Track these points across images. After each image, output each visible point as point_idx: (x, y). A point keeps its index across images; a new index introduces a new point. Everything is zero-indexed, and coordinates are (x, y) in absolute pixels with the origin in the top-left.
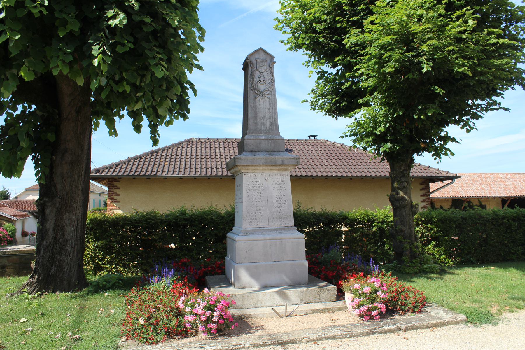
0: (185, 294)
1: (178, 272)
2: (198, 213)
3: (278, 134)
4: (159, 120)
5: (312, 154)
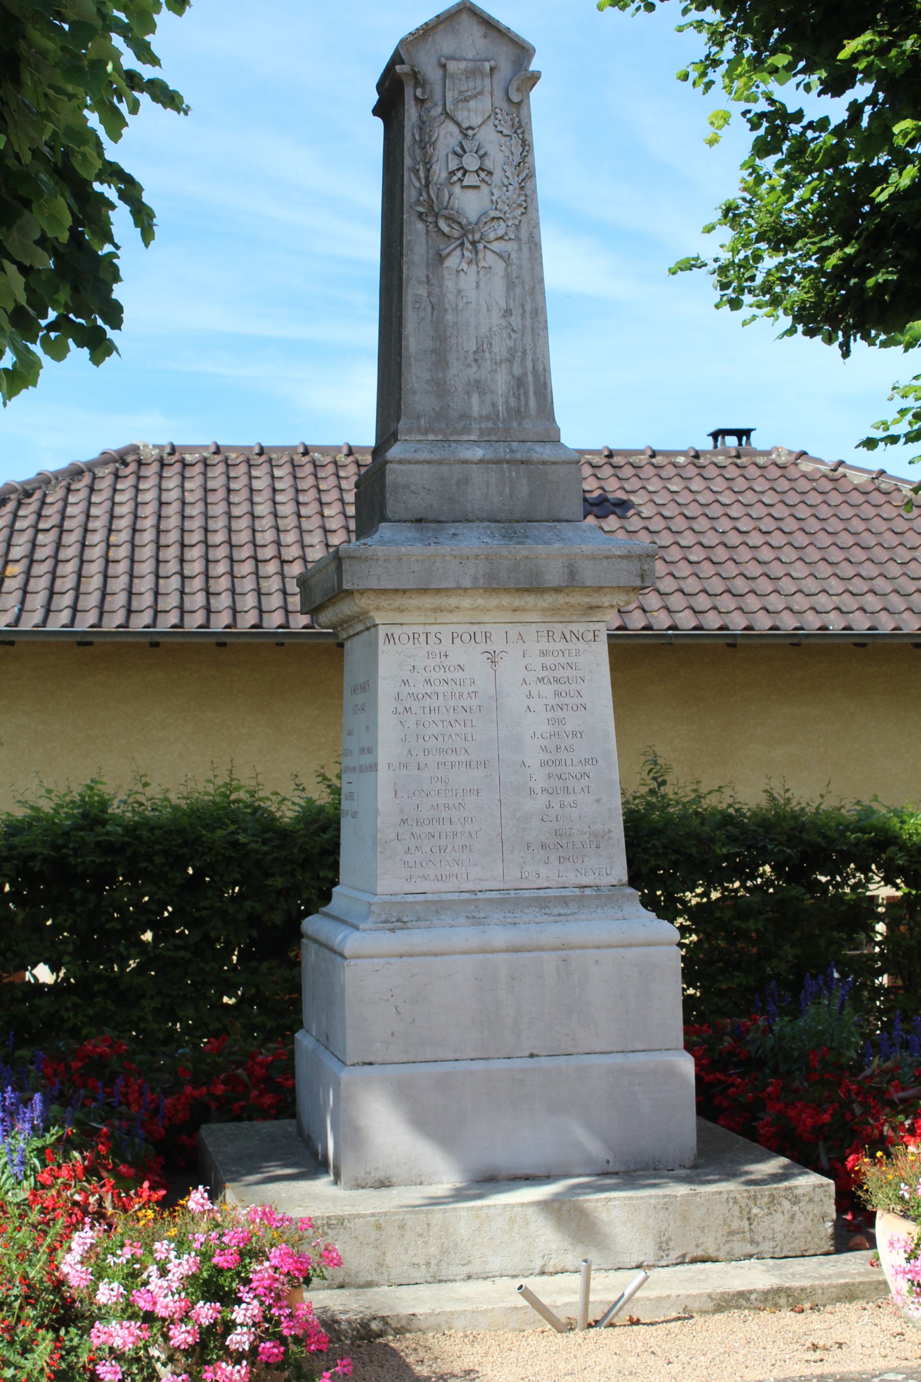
0: (100, 1215)
3: (552, 437)
5: (724, 524)
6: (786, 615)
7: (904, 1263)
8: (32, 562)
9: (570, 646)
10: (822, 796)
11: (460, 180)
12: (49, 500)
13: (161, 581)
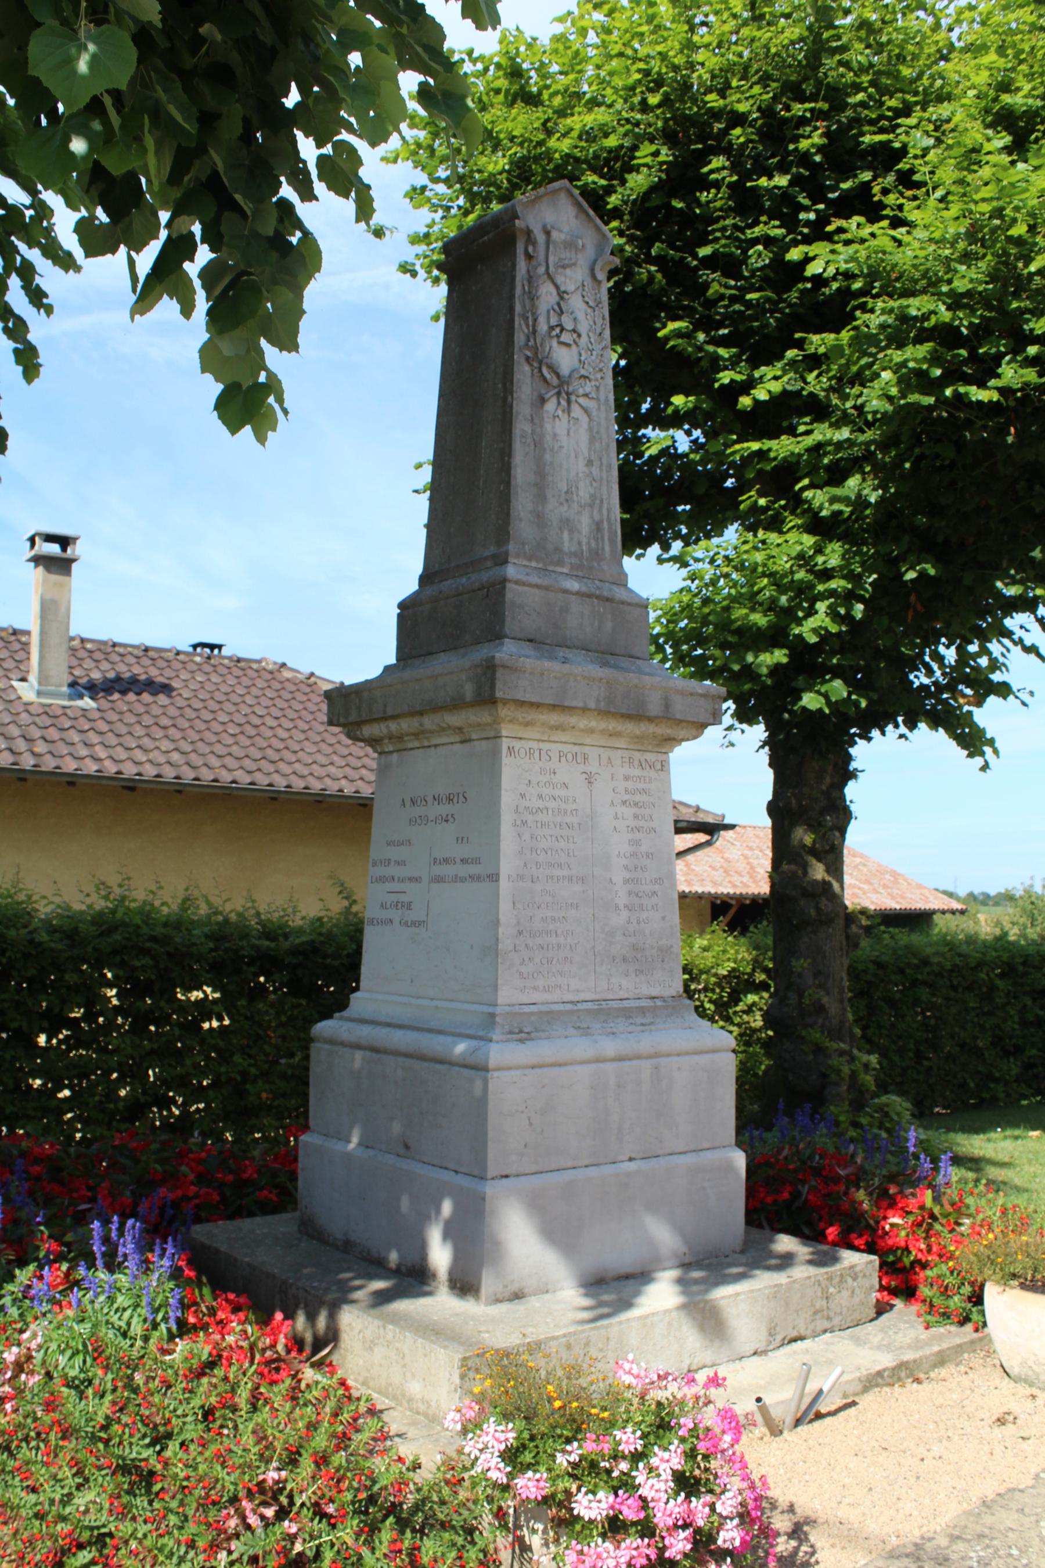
11: (558, 336)
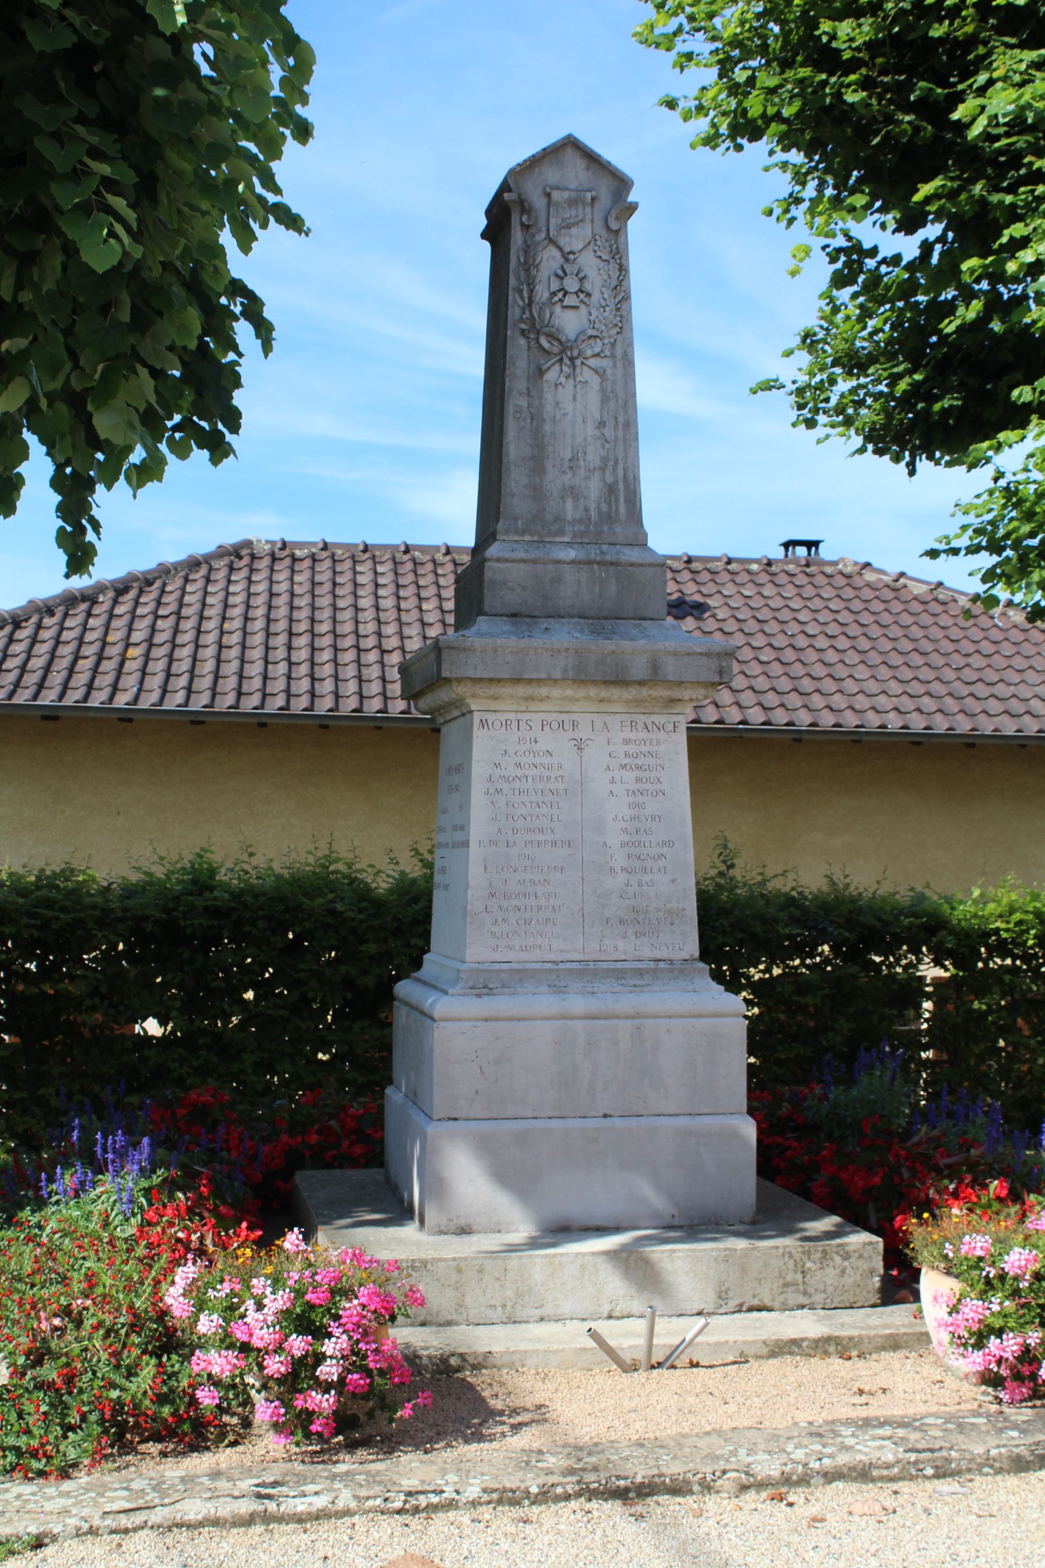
1: (170, 1149)
2: (270, 881)
3: (640, 541)
4: (100, 456)
5: (793, 628)
6: (848, 714)
7: (946, 1317)
8: (151, 645)
9: (651, 735)
10: (878, 882)
11: (561, 301)
12: (168, 589)
13: (270, 667)
